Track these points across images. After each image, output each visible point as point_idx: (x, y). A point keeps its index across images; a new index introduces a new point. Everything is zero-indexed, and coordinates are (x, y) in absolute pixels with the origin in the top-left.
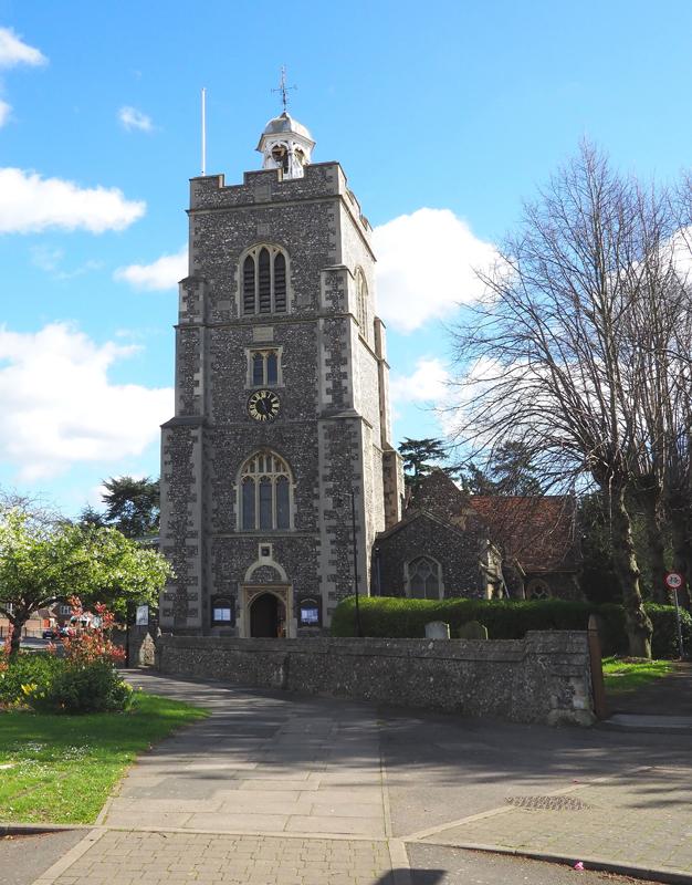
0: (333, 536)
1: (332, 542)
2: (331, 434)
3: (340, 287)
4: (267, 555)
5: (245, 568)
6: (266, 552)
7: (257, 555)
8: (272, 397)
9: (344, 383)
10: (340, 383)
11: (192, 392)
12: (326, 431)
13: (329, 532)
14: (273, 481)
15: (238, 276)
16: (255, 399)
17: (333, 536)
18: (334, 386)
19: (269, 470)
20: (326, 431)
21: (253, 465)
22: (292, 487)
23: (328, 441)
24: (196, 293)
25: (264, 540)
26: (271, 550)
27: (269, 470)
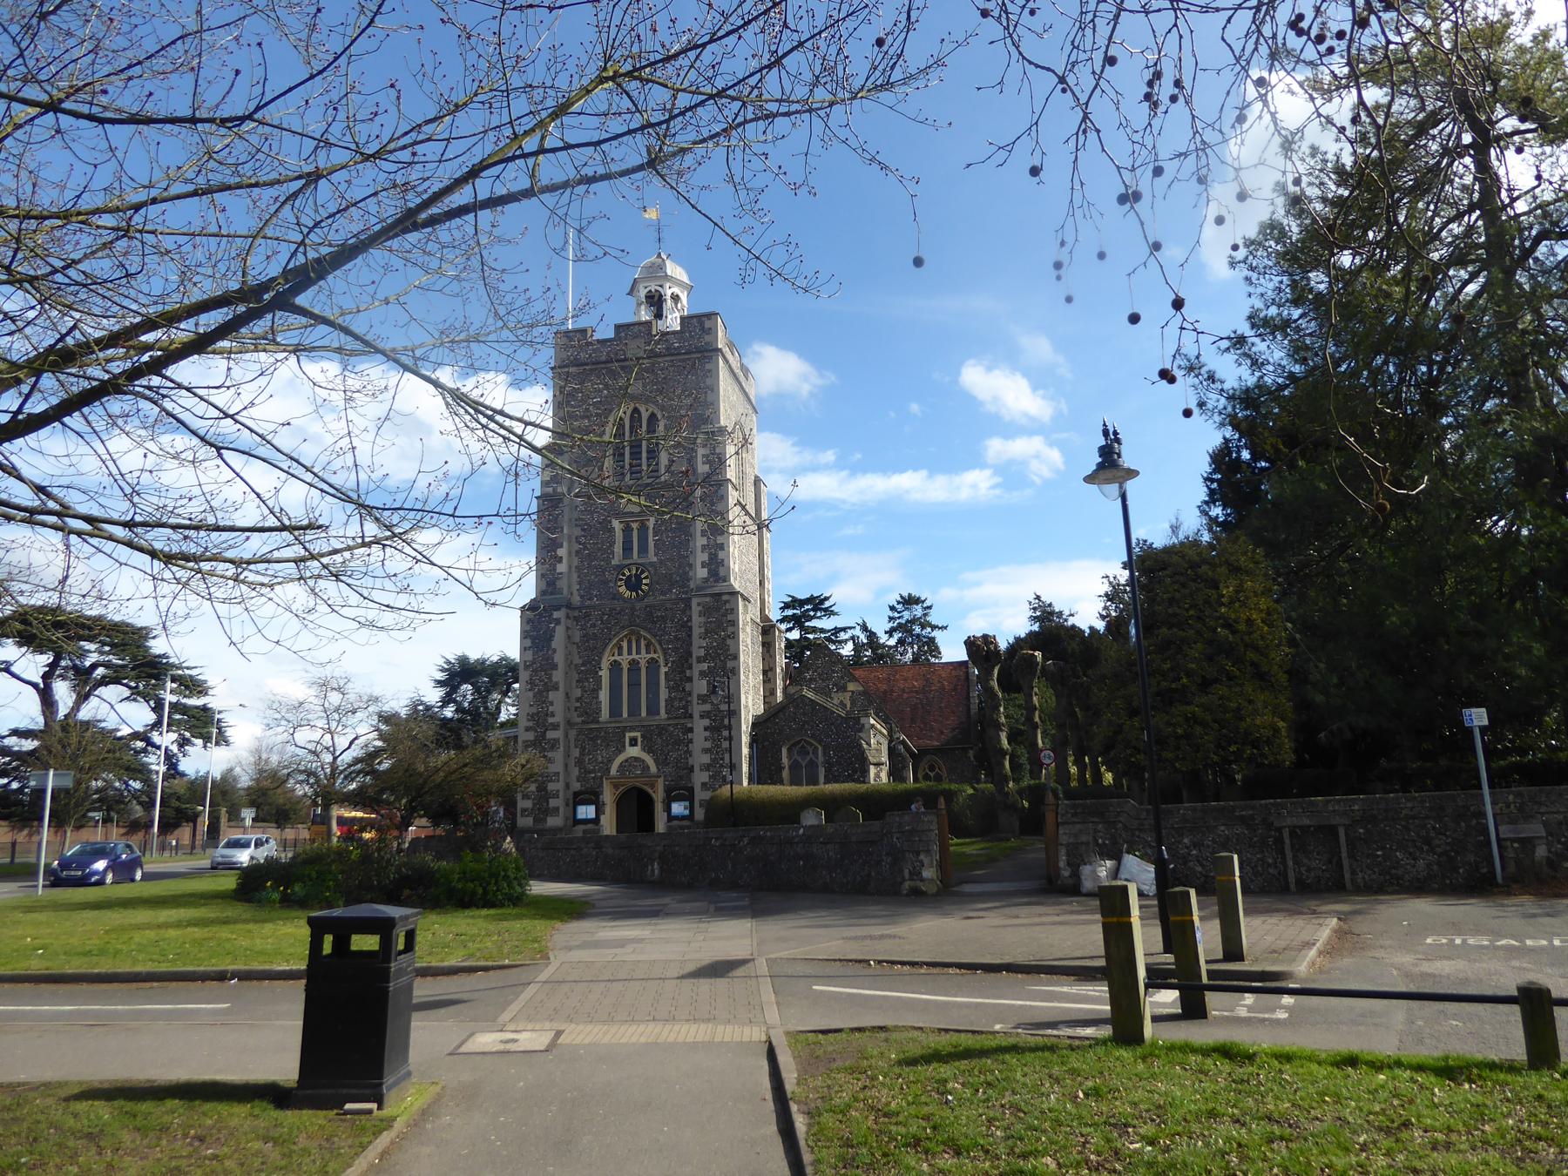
0: (706, 722)
1: (706, 729)
2: (706, 611)
3: (717, 451)
4: (636, 745)
5: (611, 761)
6: (633, 742)
7: (624, 746)
8: (642, 572)
9: (721, 555)
10: (716, 555)
12: (700, 608)
13: (702, 717)
14: (643, 664)
16: (624, 575)
17: (706, 722)
18: (710, 559)
19: (638, 652)
20: (700, 608)
21: (620, 648)
22: (663, 670)
23: (702, 619)
25: (632, 729)
26: (639, 740)
27: (638, 652)
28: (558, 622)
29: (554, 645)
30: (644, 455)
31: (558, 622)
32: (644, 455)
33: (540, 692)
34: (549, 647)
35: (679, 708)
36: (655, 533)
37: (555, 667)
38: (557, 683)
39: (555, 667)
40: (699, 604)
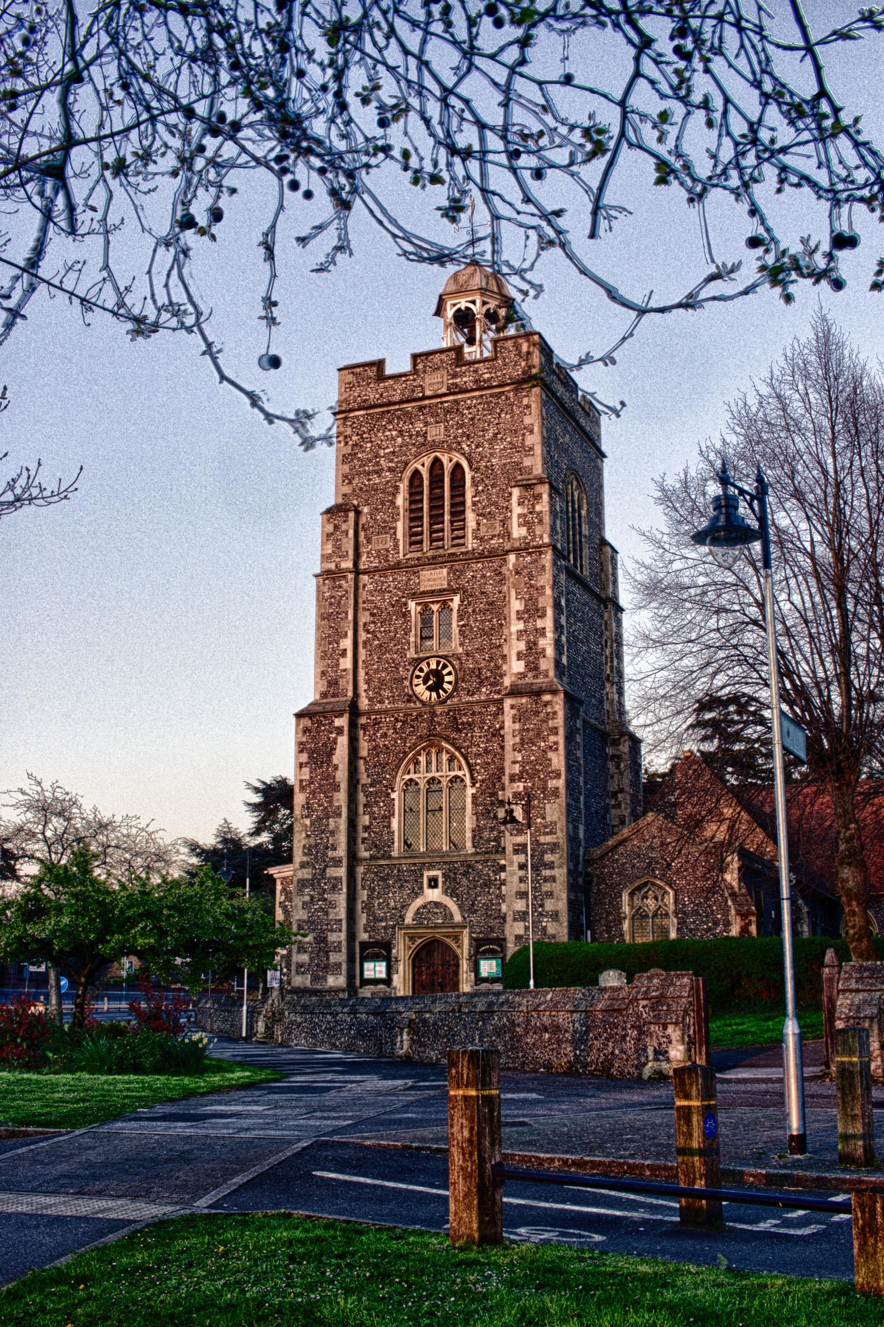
8: (445, 667)
10: (535, 644)
11: (337, 665)
15: (401, 500)
16: (421, 670)
24: (344, 527)
28: (340, 731)
29: (335, 760)
30: (447, 517)
31: (340, 731)
32: (447, 517)
33: (320, 819)
34: (329, 761)
35: (489, 841)
36: (460, 618)
37: (337, 788)
38: (339, 807)
39: (337, 788)
40: (512, 707)
